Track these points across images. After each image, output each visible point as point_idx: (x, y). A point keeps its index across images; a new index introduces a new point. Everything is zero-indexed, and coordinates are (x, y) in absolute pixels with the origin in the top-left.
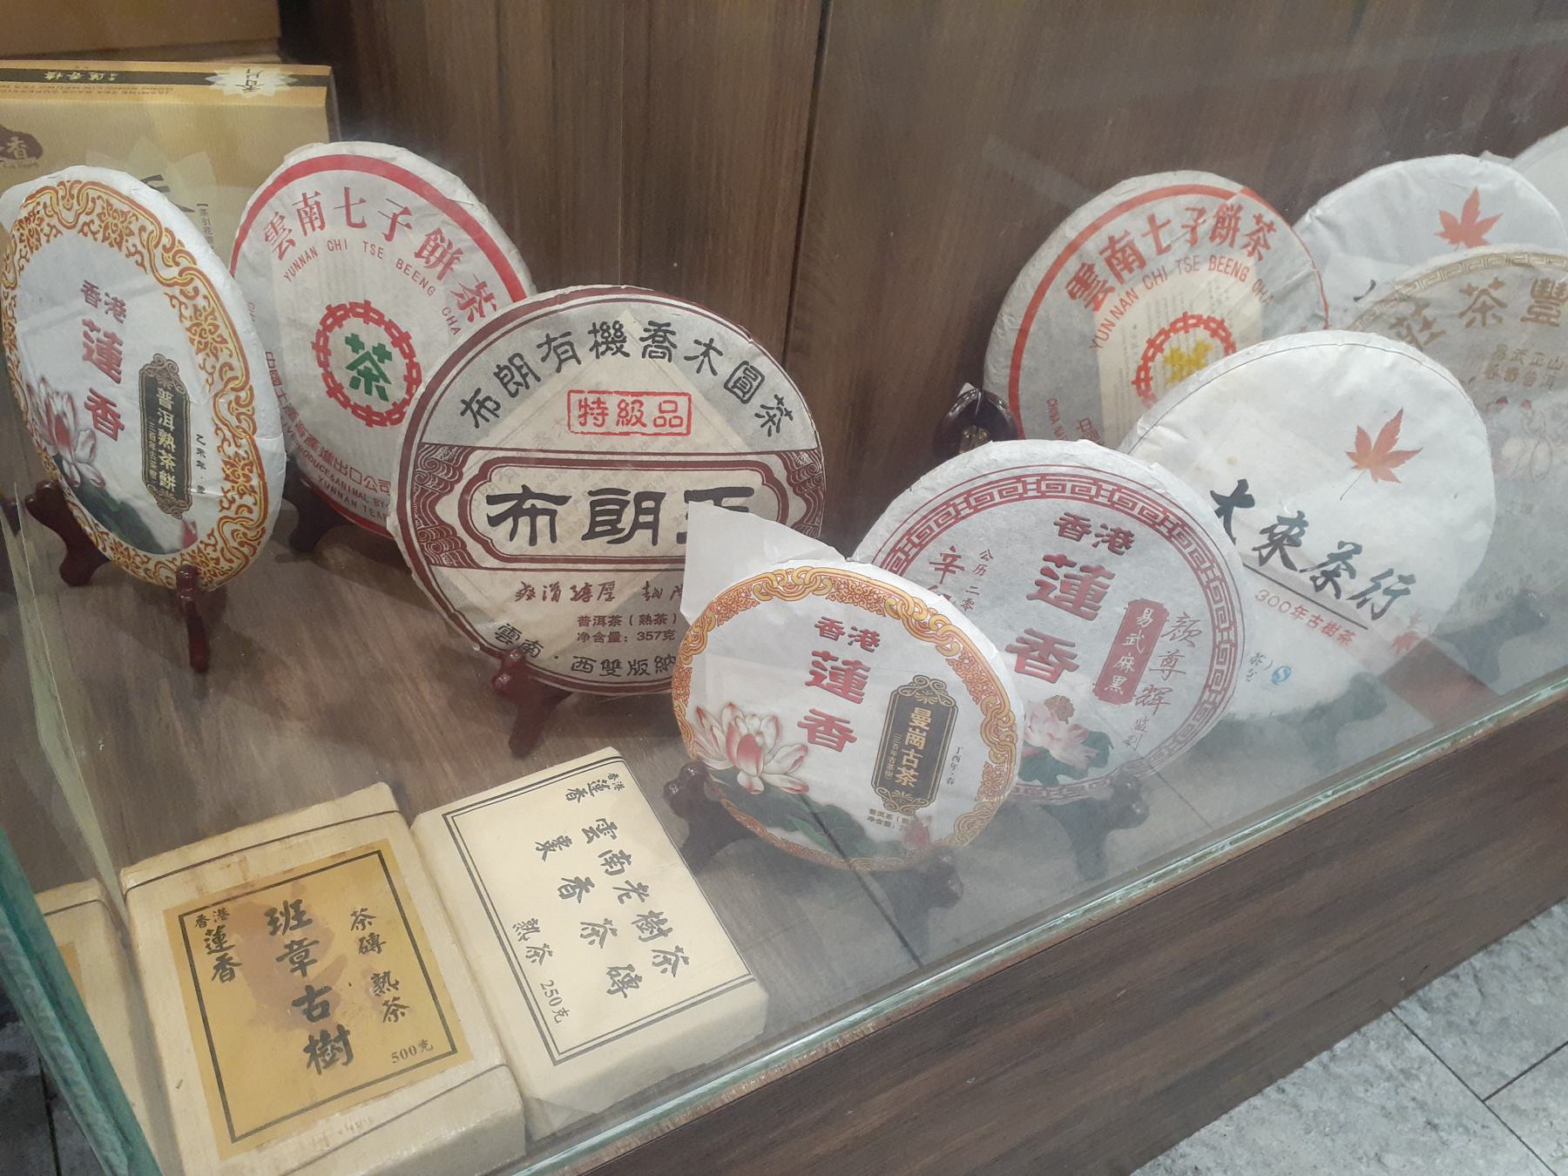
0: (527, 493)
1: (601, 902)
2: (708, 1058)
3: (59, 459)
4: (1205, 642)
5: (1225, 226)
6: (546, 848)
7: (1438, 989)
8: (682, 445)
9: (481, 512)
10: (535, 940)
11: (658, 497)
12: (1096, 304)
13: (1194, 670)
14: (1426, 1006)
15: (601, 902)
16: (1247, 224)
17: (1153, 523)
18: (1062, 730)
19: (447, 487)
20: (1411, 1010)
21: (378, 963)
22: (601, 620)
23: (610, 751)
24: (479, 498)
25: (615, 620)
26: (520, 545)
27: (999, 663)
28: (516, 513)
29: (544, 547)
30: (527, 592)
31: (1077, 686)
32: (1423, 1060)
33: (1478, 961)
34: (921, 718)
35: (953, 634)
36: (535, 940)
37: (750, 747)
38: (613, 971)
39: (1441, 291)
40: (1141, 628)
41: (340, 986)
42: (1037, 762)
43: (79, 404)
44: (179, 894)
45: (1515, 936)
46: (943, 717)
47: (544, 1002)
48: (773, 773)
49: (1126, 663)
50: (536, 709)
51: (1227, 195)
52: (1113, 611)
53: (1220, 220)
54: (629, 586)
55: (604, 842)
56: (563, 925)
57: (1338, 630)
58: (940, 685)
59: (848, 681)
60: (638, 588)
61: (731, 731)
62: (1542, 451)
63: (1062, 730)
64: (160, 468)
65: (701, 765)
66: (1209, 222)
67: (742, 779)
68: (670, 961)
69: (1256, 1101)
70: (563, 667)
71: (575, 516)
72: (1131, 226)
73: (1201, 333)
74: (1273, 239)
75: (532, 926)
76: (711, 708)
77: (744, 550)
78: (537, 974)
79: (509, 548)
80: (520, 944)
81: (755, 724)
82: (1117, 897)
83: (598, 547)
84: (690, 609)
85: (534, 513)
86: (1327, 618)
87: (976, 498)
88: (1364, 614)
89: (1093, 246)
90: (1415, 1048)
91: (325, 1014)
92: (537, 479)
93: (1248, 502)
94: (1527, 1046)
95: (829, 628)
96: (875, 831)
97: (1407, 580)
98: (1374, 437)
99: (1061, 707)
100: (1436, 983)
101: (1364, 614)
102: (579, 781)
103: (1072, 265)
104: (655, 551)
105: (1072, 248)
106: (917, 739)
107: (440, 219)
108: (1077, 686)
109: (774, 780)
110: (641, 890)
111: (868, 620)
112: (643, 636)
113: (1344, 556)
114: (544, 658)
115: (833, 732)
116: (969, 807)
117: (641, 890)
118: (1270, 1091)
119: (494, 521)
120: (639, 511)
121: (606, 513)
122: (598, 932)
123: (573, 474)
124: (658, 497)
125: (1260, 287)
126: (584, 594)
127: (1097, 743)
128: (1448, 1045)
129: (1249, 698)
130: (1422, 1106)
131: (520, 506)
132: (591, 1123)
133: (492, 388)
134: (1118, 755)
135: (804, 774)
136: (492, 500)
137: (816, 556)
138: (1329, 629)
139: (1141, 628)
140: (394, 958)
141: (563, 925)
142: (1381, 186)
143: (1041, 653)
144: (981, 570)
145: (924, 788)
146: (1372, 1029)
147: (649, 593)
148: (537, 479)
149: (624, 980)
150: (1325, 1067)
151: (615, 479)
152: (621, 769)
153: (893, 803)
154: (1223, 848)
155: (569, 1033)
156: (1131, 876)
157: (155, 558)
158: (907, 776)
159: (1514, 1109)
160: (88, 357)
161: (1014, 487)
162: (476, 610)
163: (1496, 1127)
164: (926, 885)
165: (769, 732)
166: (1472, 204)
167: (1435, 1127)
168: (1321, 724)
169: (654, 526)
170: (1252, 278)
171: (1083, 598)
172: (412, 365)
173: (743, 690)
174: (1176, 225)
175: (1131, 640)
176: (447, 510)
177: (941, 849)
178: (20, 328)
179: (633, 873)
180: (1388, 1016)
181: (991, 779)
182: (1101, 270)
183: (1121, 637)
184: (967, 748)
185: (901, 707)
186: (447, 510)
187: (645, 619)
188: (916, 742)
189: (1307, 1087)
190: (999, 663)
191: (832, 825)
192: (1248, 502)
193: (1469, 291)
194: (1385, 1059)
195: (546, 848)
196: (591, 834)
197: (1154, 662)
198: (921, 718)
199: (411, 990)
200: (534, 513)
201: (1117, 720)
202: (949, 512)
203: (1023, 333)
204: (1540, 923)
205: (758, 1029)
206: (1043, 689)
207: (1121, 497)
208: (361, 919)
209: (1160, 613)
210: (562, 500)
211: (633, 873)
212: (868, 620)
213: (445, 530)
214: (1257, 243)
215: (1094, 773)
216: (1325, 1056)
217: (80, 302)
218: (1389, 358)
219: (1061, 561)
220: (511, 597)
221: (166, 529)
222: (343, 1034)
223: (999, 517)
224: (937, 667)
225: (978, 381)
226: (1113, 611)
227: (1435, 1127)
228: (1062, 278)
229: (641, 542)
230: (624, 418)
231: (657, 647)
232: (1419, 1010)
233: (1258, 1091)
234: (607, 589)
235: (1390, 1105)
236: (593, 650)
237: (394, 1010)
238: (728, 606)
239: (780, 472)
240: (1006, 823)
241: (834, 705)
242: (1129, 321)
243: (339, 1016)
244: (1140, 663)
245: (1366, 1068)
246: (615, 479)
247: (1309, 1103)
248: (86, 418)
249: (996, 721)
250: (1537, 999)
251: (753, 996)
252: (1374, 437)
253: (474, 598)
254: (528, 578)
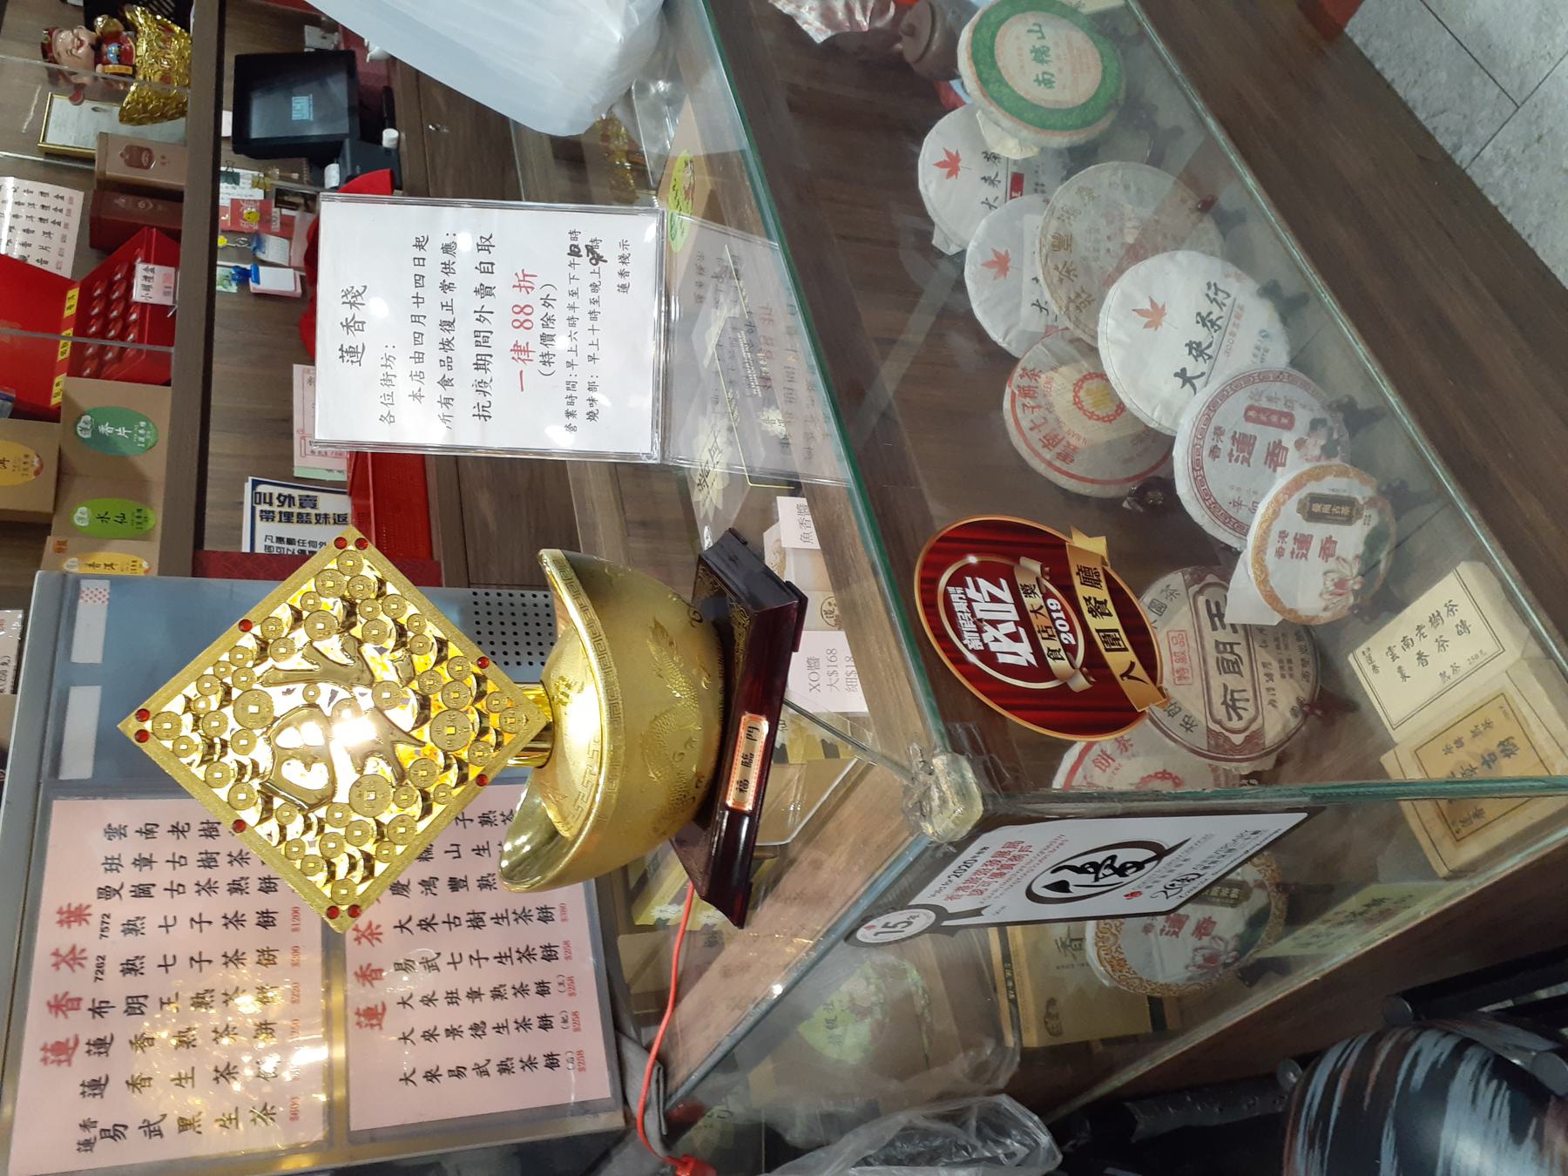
0: (1224, 703)
1: (1427, 646)
2: (1498, 585)
3: (1226, 965)
4: (1261, 386)
5: (1027, 392)
6: (1404, 677)
7: (1445, 141)
8: (1191, 633)
9: (1236, 724)
10: (1449, 672)
11: (1217, 643)
12: (1075, 449)
13: (1276, 388)
14: (1457, 148)
15: (1427, 646)
16: (1025, 382)
17: (1209, 419)
18: (1310, 442)
19: (1227, 739)
20: (1462, 157)
21: (1467, 736)
22: (1282, 668)
23: (1351, 658)
24: (1229, 725)
25: (1280, 661)
26: (1250, 706)
27: (1283, 478)
28: (1235, 709)
29: (1249, 695)
30: (1273, 703)
31: (1288, 439)
32: (1494, 148)
33: (1421, 116)
34: (1317, 508)
35: (1276, 499)
36: (1449, 672)
37: (1341, 584)
38: (1460, 633)
39: (1062, 293)
40: (1257, 414)
41: (1480, 751)
42: (1328, 451)
43: (1199, 944)
44: (1447, 845)
45: (1401, 93)
46: (1315, 498)
47: (1477, 661)
48: (1352, 571)
49: (1274, 418)
50: (1333, 705)
51: (1013, 394)
52: (1250, 429)
53: (1026, 396)
54: (1262, 655)
55: (1398, 651)
56: (1440, 662)
57: (1238, 312)
58: (1300, 502)
59: (1303, 541)
60: (1263, 651)
61: (1332, 594)
62: (1129, 224)
63: (1310, 442)
64: (1228, 897)
65: (1352, 608)
66: (1028, 401)
67: (1357, 587)
68: (1451, 608)
69: (1539, 253)
70: (1308, 687)
71: (1231, 680)
72: (1035, 437)
73: (1082, 394)
74: (1030, 367)
75: (1443, 675)
76: (1323, 604)
77: (1244, 598)
78: (1465, 668)
79: (1252, 711)
80: (1450, 680)
81: (1329, 583)
82: (1393, 399)
83: (1245, 669)
84: (1274, 619)
85: (1233, 700)
86: (1233, 319)
87: (1206, 497)
88: (1228, 302)
89: (1048, 455)
90: (1488, 153)
91: (1493, 754)
92: (1217, 699)
93: (1184, 370)
94: (1476, 81)
95: (1280, 553)
96: (1375, 521)
97: (1209, 285)
98: (1146, 320)
99: (1300, 444)
100: (1441, 141)
101: (1228, 302)
102: (1368, 669)
103: (1058, 463)
104: (1244, 643)
105: (1049, 464)
106: (1326, 509)
107: (1087, 760)
108: (1288, 439)
109: (1355, 571)
110: (1419, 628)
111: (1274, 535)
112: (1287, 647)
113: (1203, 320)
114: (1305, 696)
115: (1328, 549)
116: (1356, 482)
117: (1419, 628)
118: (1531, 244)
119: (1240, 718)
120: (1225, 651)
121: (1230, 666)
122: (1442, 644)
123: (1212, 683)
124: (1217, 643)
125: (1054, 369)
126: (1270, 676)
127: (1315, 425)
128: (1482, 132)
129: (1279, 357)
130: (1527, 146)
131: (1231, 706)
132: (1535, 634)
133: (1179, 718)
134: (1320, 414)
135: (1350, 557)
136: (1230, 719)
137: (1245, 564)
138: (1238, 317)
139: (1257, 414)
140: (1464, 731)
141: (1440, 662)
142: (985, 312)
143: (1275, 456)
144: (1239, 489)
145: (1350, 502)
146: (1478, 182)
147: (1264, 645)
148: (1217, 699)
149: (1463, 627)
150: (1509, 210)
151: (1212, 663)
152: (1358, 652)
153: (1359, 515)
154: (1361, 350)
155: (1490, 647)
156: (1381, 393)
157: (1273, 909)
158: (1345, 510)
159: (1520, 88)
160: (1176, 934)
161: (1199, 480)
162: (1284, 727)
163: (1534, 98)
164: (1397, 498)
165: (1331, 575)
166: (989, 265)
167: (1540, 137)
168: (1289, 307)
169: (1231, 644)
170: (1051, 374)
171: (1244, 443)
172: (1156, 776)
173: (1311, 592)
174: (1032, 417)
175: (1263, 418)
176: (1238, 739)
177: (1379, 490)
178: (1161, 979)
179: (1412, 634)
180: (1469, 172)
181: (1342, 473)
182: (1059, 449)
183: (1263, 423)
184: (1330, 485)
185: (1312, 517)
186: (1238, 739)
187: (1278, 647)
188: (1320, 509)
189: (1525, 221)
190: (1283, 478)
191: (1373, 542)
192: (1184, 370)
193: (1061, 280)
194: (1498, 172)
195: (1404, 677)
196: (1394, 658)
197: (1273, 407)
198: (1317, 508)
199: (1478, 719)
200: (1233, 700)
201: (1303, 419)
202: (1213, 507)
203: (1093, 481)
204: (1388, 75)
205: (1482, 565)
206: (1292, 454)
207: (1200, 433)
208: (1448, 750)
209: (1250, 408)
210: (1225, 687)
211: (1412, 634)
212: (1274, 535)
213: (1248, 740)
214: (1033, 375)
215: (1330, 423)
216: (1501, 210)
217: (1151, 935)
218: (1110, 321)
219: (1231, 455)
220: (1276, 709)
221: (1258, 899)
222: (1501, 743)
223: (1213, 486)
224: (1292, 505)
225: (1122, 499)
226: (1250, 429)
227: (1540, 137)
228: (1064, 467)
229: (1240, 650)
230: (1183, 660)
231: (1291, 640)
232: (1461, 152)
233: (1532, 251)
234: (1264, 665)
235: (1529, 166)
236: (1298, 671)
237: (1488, 725)
238: (1273, 599)
239: (1196, 588)
240: (1361, 462)
241: (1315, 546)
242: (1083, 432)
243: (1494, 747)
244: (1273, 412)
245: (1506, 184)
246: (1212, 663)
247: (1534, 219)
248: (1206, 940)
249: (1316, 475)
250: (1443, 76)
251: (1464, 568)
252: (1146, 320)
253: (1279, 728)
254: (1265, 703)
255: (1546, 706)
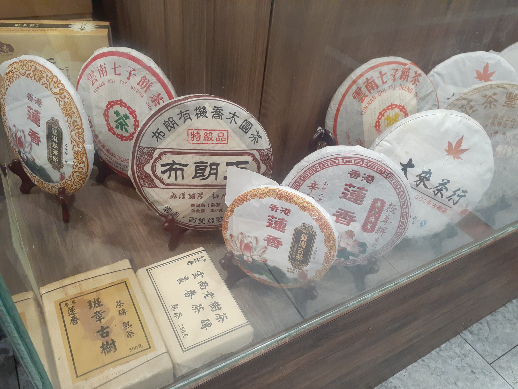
0: (174, 163)
1: (199, 298)
2: (234, 350)
3: (19, 152)
4: (398, 212)
5: (405, 75)
6: (180, 280)
7: (475, 327)
8: (225, 147)
9: (159, 169)
10: (177, 311)
11: (217, 165)
12: (362, 100)
13: (395, 222)
14: (471, 333)
15: (199, 298)
16: (412, 74)
17: (381, 173)
18: (351, 242)
19: (148, 161)
20: (466, 334)
21: (125, 318)
22: (198, 205)
23: (201, 249)
24: (158, 165)
25: (203, 205)
26: (172, 180)
27: (330, 219)
28: (170, 170)
29: (180, 181)
30: (174, 196)
31: (356, 227)
32: (470, 351)
33: (488, 318)
34: (304, 238)
35: (315, 210)
36: (177, 311)
37: (248, 247)
38: (202, 321)
39: (476, 96)
40: (377, 208)
41: (112, 326)
42: (342, 252)
43: (26, 134)
44: (59, 296)
45: (501, 310)
46: (312, 237)
47: (180, 331)
48: (255, 256)
49: (372, 219)
50: (177, 235)
51: (405, 64)
52: (368, 202)
53: (403, 73)
54: (208, 194)
55: (199, 279)
56: (186, 306)
57: (442, 208)
58: (310, 227)
59: (280, 225)
60: (211, 194)
61: (241, 242)
62: (509, 149)
63: (351, 242)
64: (53, 155)
65: (231, 253)
66: (399, 73)
67: (245, 258)
68: (221, 318)
69: (415, 364)
70: (186, 221)
71: (190, 171)
72: (374, 75)
73: (397, 110)
74: (420, 79)
75: (176, 306)
76: (235, 234)
77: (246, 182)
78: (178, 322)
79: (168, 181)
80: (172, 312)
81: (249, 239)
82: (369, 297)
83: (197, 181)
84: (228, 202)
85: (176, 170)
86: (438, 204)
87: (322, 165)
88: (451, 203)
89: (361, 81)
90: (468, 347)
91: (107, 335)
92: (177, 158)
93: (412, 166)
94: (505, 346)
95: (274, 208)
96: (289, 275)
97: (465, 192)
98: (454, 144)
99: (351, 234)
100: (474, 325)
101: (451, 203)
102: (191, 258)
103: (354, 88)
104: (216, 182)
105: (354, 82)
106: (303, 244)
107: (145, 73)
108: (356, 227)
109: (256, 258)
110: (212, 294)
111: (287, 205)
112: (212, 210)
113: (444, 184)
114: (180, 218)
115: (275, 242)
116: (320, 267)
117: (212, 294)
118: (420, 361)
119: (163, 172)
120: (211, 169)
121: (200, 170)
122: (197, 308)
123: (189, 157)
124: (217, 165)
125: (416, 95)
126: (193, 197)
127: (363, 246)
128: (478, 346)
129: (413, 231)
130: (470, 366)
131: (172, 168)
132: (195, 371)
133: (163, 128)
134: (369, 250)
135: (265, 256)
136: (163, 165)
137: (270, 184)
138: (439, 208)
139: (377, 208)
140: (130, 317)
141: (186, 306)
142: (456, 61)
143: (344, 216)
144: (324, 189)
145: (305, 261)
146: (453, 340)
147: (214, 196)
148: (177, 158)
149: (206, 324)
150: (438, 353)
151: (203, 158)
152: (205, 254)
153: (295, 266)
154: (404, 281)
155: (188, 342)
156: (373, 290)
157: (51, 184)
158: (300, 257)
159: (500, 367)
160: (29, 118)
161: (335, 161)
162: (157, 202)
163: (494, 373)
164: (306, 293)
165: (254, 242)
166: (486, 67)
167: (474, 373)
168: (436, 239)
169: (216, 174)
170: (414, 92)
171: (358, 198)
172: (136, 121)
173: (245, 228)
174: (388, 74)
175: (374, 212)
176: (148, 169)
177: (311, 281)
178: (7, 109)
179: (209, 289)
180: (458, 336)
181: (327, 258)
182: (364, 89)
183: (370, 211)
184: (320, 247)
185: (298, 234)
186: (148, 169)
187: (213, 205)
188: (303, 246)
189: (432, 360)
190: (330, 219)
191: (275, 273)
192: (412, 166)
193: (485, 96)
194: (458, 350)
195: (180, 280)
196: (195, 276)
197: (381, 219)
198: (304, 238)
199: (136, 327)
200: (176, 170)
201: (369, 238)
202: (313, 169)
203: (338, 110)
204: (509, 305)
205: (250, 340)
206: (345, 228)
207: (370, 164)
208: (119, 304)
209: (383, 203)
210: (186, 165)
211: (209, 289)
212: (287, 205)
213: (147, 175)
214: (415, 80)
215: (361, 256)
216: (438, 349)
217: (27, 100)
218: (459, 118)
219: (351, 186)
220: (169, 197)
221: (55, 175)
222: (113, 342)
223: (330, 171)
224: (310, 221)
225: (323, 126)
226: (368, 202)
227: (474, 373)
228: (351, 92)
229: (212, 179)
230: (206, 138)
231: (217, 214)
232: (469, 334)
233: (416, 361)
234: (201, 195)
235: (459, 366)
236: (196, 215)
237: (130, 334)
238: (241, 200)
239: (258, 156)
240: (332, 272)
241: (276, 233)
242: (373, 106)
243: (112, 336)
244: (377, 219)
245: (451, 353)
246: (203, 158)
247: (433, 365)
248: (29, 138)
249: (329, 238)
250: (508, 331)
251: (249, 329)
252: (454, 144)
253: (156, 198)
254: (174, 191)
255: (146, 374)
